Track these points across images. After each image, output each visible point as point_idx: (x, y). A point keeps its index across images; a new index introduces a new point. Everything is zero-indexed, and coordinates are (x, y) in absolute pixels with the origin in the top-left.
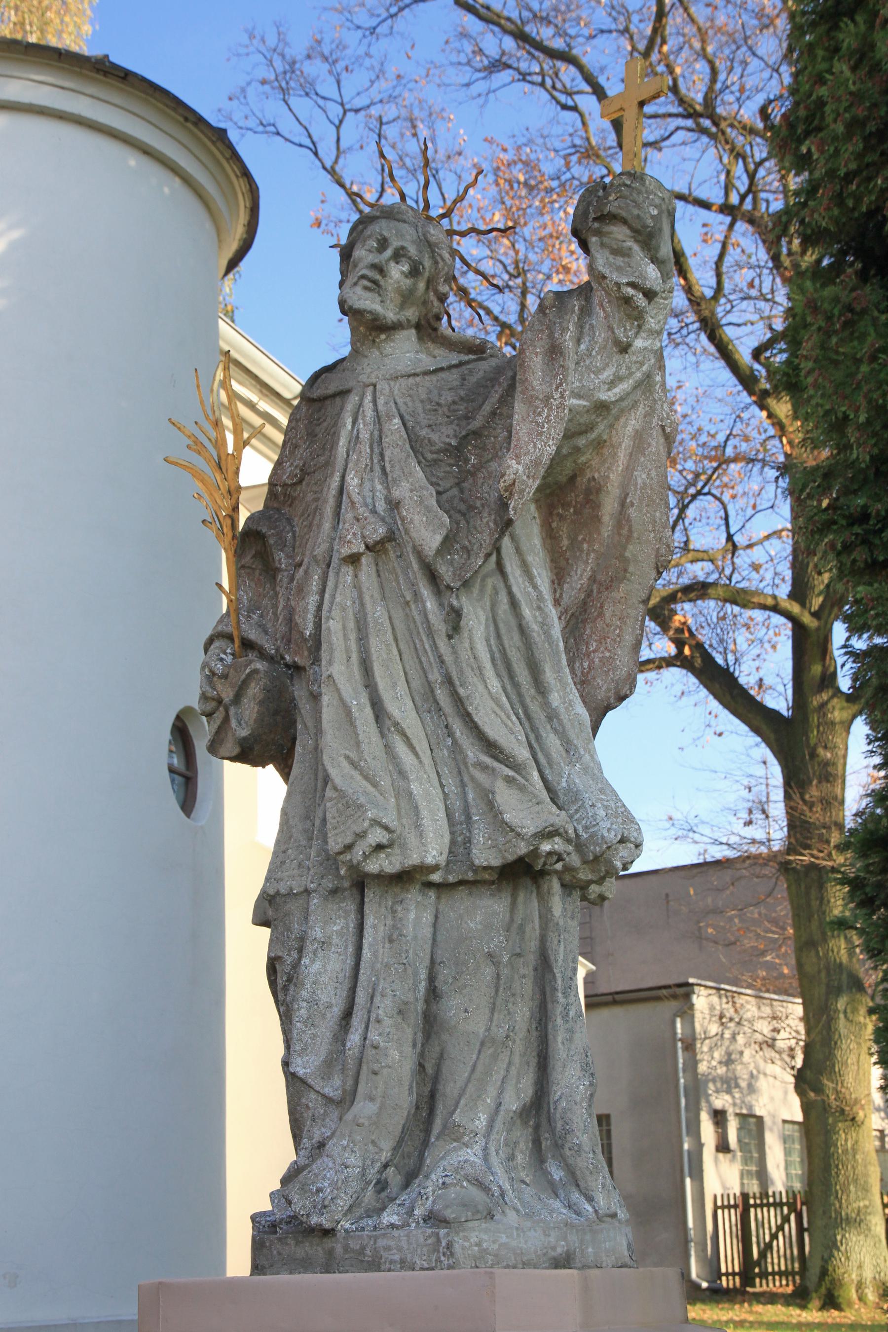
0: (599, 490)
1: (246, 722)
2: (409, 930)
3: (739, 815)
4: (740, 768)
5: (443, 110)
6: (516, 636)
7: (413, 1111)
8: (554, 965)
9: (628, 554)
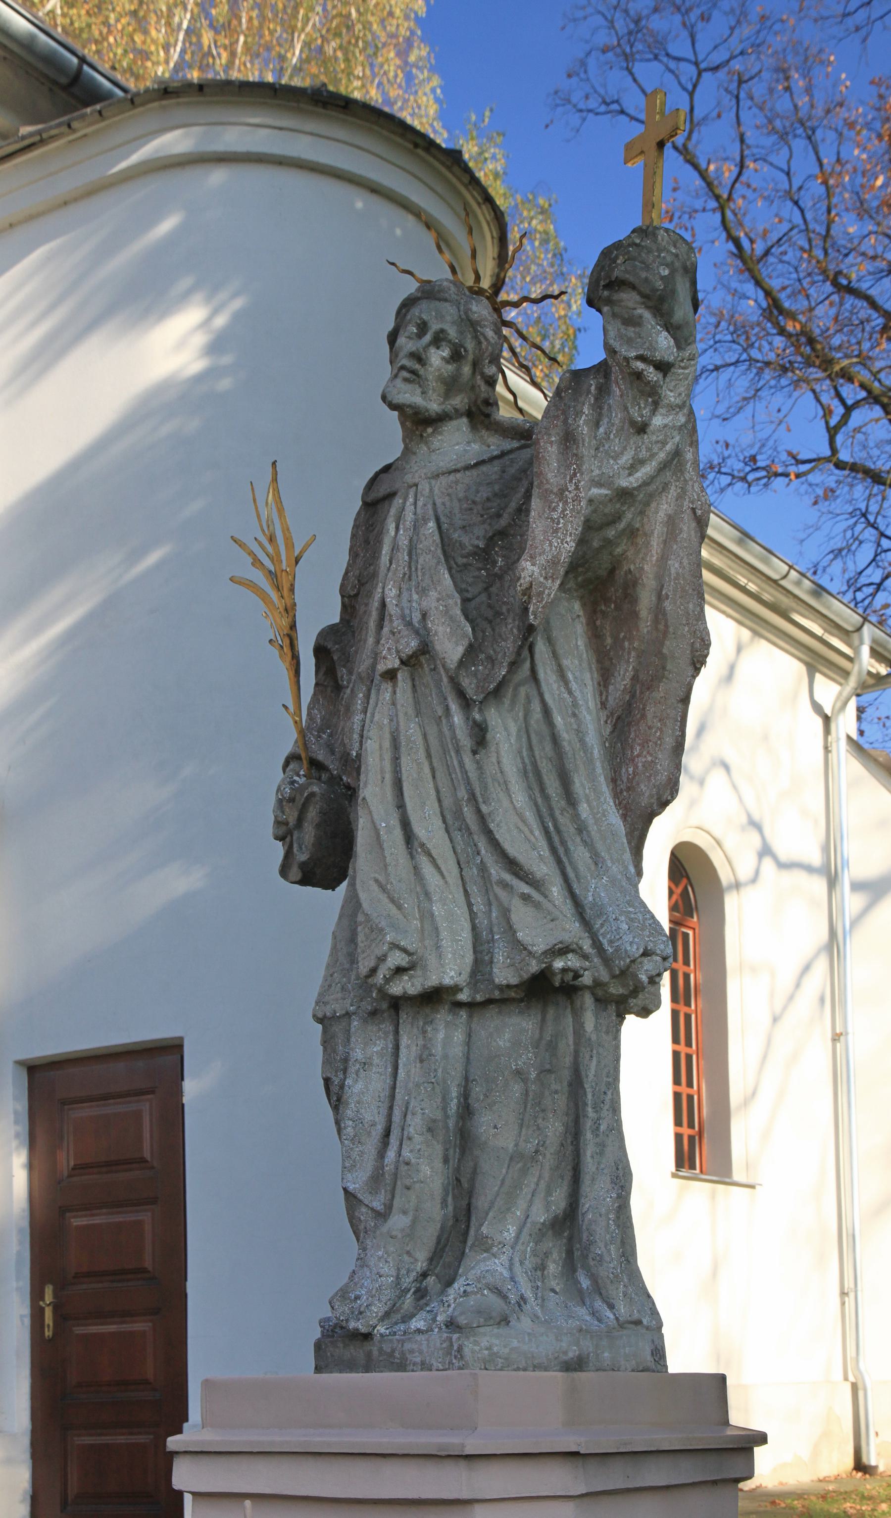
0: (635, 583)
2: (438, 1050)
5: (821, 51)
7: (450, 1223)
8: (585, 1080)
9: (665, 651)
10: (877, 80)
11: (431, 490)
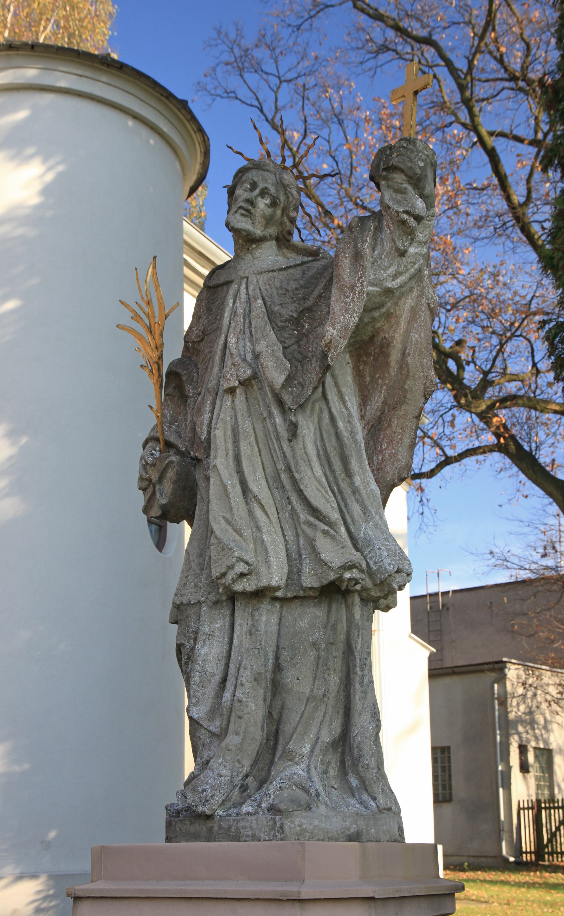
0: (388, 345)
1: (166, 495)
2: (262, 627)
3: (538, 550)
4: (538, 519)
6: (334, 440)
7: (265, 741)
8: (355, 650)
9: (406, 387)
10: (377, 98)
11: (258, 281)
